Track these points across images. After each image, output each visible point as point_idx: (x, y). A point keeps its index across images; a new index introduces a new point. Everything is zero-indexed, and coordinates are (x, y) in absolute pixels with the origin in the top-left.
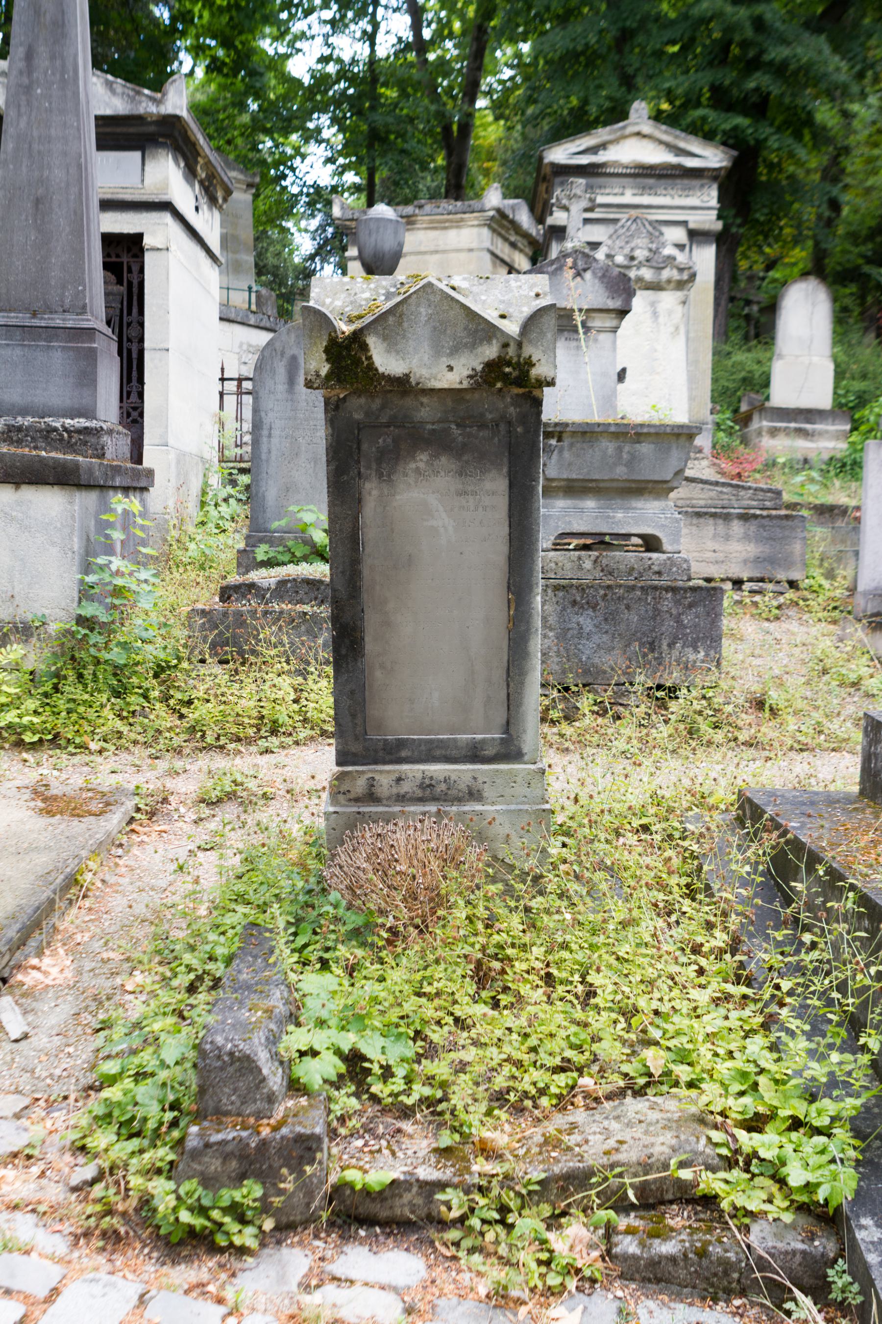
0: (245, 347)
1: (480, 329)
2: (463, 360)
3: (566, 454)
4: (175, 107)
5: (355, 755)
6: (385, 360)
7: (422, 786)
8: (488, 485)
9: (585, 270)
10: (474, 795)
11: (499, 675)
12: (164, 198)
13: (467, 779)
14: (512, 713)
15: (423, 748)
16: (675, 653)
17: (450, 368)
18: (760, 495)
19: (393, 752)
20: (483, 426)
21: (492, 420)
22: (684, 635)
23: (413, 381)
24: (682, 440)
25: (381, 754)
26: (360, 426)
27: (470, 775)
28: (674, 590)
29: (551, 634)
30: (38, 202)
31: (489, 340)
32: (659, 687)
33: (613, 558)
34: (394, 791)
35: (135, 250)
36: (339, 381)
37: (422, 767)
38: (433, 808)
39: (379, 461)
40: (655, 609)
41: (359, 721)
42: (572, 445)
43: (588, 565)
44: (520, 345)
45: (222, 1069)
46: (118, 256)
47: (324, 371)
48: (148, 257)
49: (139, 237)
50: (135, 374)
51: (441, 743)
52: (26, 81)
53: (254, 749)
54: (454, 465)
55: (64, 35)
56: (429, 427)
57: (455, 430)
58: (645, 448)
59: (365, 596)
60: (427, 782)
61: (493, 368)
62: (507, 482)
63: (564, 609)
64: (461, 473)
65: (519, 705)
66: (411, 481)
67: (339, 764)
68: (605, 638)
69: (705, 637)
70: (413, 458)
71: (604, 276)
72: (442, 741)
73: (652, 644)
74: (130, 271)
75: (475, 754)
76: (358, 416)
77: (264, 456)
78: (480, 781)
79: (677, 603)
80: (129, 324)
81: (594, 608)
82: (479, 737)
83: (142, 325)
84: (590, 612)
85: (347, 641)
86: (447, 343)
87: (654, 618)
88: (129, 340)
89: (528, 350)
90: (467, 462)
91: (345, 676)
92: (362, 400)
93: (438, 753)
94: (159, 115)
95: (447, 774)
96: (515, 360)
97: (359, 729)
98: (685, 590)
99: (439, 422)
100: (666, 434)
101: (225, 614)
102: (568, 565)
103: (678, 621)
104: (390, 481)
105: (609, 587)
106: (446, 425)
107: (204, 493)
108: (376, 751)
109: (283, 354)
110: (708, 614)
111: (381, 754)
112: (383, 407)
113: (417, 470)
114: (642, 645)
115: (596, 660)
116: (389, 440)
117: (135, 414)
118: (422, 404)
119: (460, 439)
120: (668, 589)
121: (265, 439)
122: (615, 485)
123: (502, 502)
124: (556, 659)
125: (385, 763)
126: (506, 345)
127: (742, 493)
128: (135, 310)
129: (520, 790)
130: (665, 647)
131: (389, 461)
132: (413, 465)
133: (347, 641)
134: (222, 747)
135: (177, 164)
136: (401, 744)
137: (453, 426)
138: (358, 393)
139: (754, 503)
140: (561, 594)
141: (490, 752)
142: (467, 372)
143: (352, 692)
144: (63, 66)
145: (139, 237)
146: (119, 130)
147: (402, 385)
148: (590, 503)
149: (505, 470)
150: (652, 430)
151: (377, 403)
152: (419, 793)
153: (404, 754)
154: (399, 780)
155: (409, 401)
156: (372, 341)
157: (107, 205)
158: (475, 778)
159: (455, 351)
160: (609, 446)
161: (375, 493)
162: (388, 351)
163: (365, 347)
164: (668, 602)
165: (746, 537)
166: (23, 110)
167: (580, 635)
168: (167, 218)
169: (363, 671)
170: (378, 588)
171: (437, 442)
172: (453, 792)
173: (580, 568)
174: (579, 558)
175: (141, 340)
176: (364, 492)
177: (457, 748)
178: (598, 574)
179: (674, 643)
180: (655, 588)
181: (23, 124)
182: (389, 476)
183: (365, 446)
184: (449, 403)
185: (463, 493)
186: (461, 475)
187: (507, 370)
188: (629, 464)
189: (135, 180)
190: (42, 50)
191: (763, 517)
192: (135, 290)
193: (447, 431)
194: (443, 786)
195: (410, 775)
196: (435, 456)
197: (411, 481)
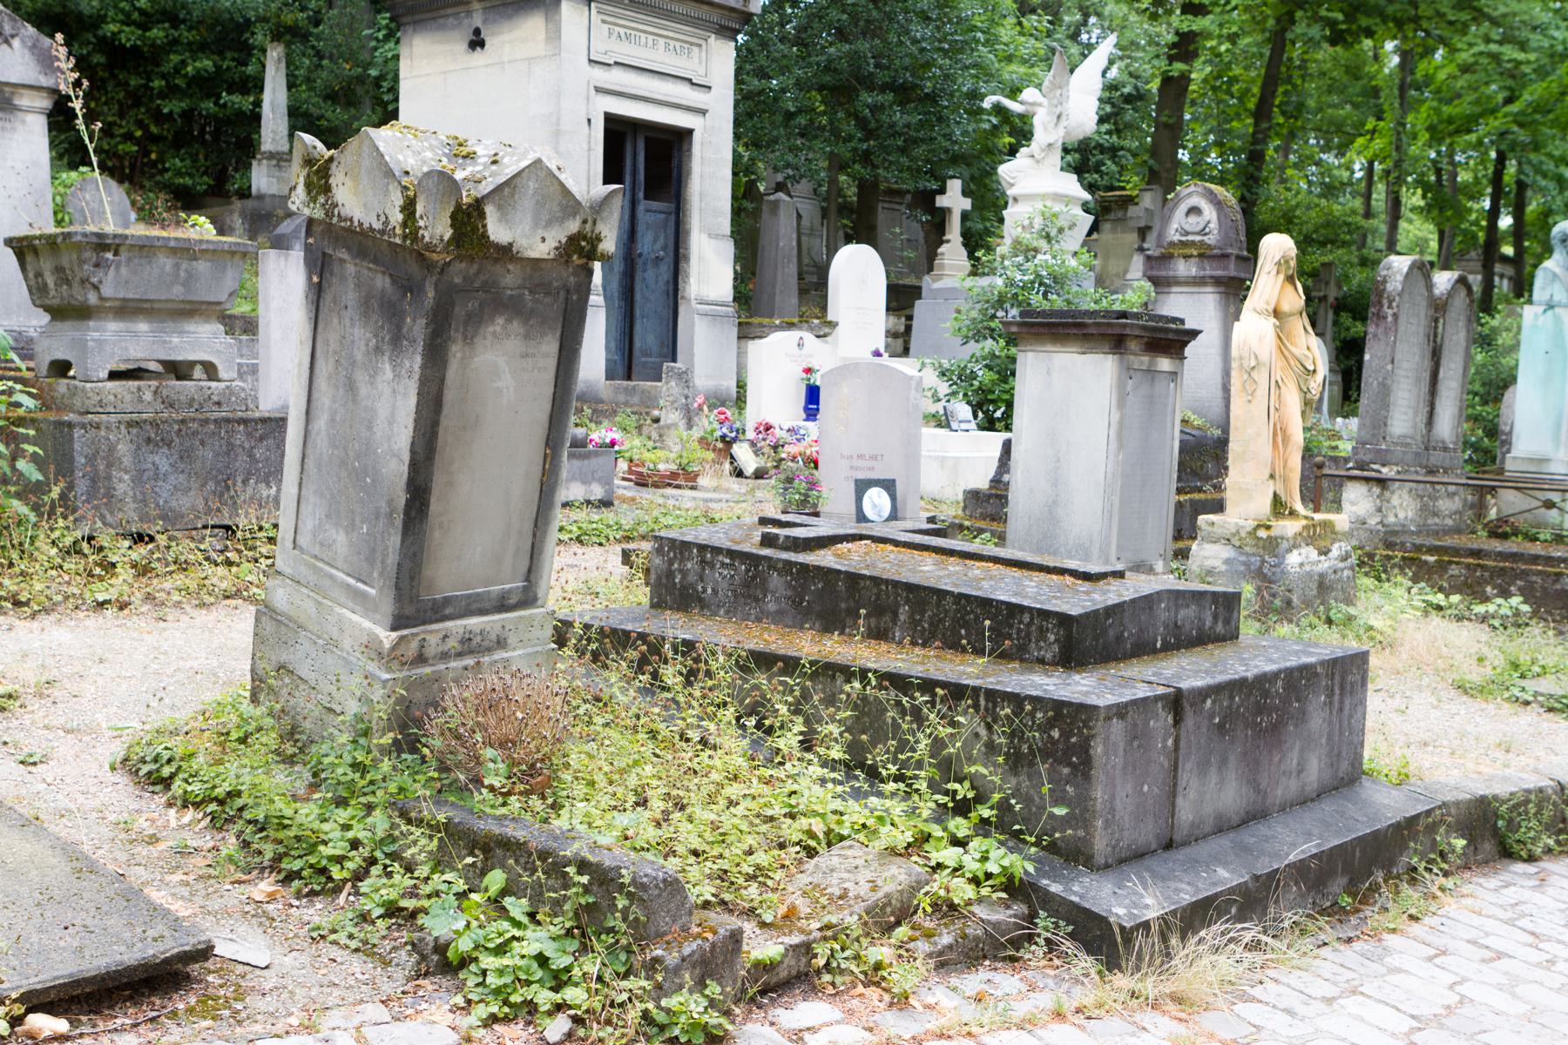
2: (553, 233)
3: (123, 270)
5: (408, 618)
6: (497, 230)
7: (462, 642)
9: (13, 36)
10: (501, 643)
13: (497, 629)
16: (249, 491)
17: (543, 239)
19: (438, 611)
20: (548, 294)
22: (258, 470)
29: (126, 477)
31: (574, 215)
33: (173, 388)
34: (440, 649)
39: (466, 324)
40: (229, 444)
42: (129, 260)
43: (148, 396)
45: (659, 896)
57: (528, 296)
58: (202, 266)
63: (138, 448)
64: (527, 337)
65: (541, 553)
68: (182, 478)
70: (493, 321)
71: (34, 46)
72: (478, 594)
75: (502, 605)
76: (457, 280)
79: (249, 435)
81: (169, 446)
82: (507, 586)
84: (165, 450)
86: (545, 216)
87: (228, 453)
92: (463, 265)
93: (474, 606)
94: (1272, 105)
102: (128, 398)
104: (472, 343)
105: (183, 421)
111: (429, 613)
112: (479, 272)
114: (218, 483)
115: (174, 504)
122: (169, 306)
123: (551, 364)
124: (133, 506)
130: (239, 484)
131: (475, 321)
132: (491, 329)
136: (447, 601)
140: (134, 431)
147: (506, 252)
148: (143, 326)
149: (558, 334)
150: (211, 247)
151: (475, 266)
152: (459, 647)
153: (447, 611)
154: (446, 637)
159: (549, 224)
160: (165, 262)
161: (459, 355)
163: (482, 215)
167: (156, 477)
171: (511, 307)
172: (486, 643)
173: (140, 400)
174: (139, 389)
178: (159, 407)
184: (528, 270)
185: (525, 356)
188: (186, 283)
193: (521, 296)
196: (509, 321)
197: (488, 343)
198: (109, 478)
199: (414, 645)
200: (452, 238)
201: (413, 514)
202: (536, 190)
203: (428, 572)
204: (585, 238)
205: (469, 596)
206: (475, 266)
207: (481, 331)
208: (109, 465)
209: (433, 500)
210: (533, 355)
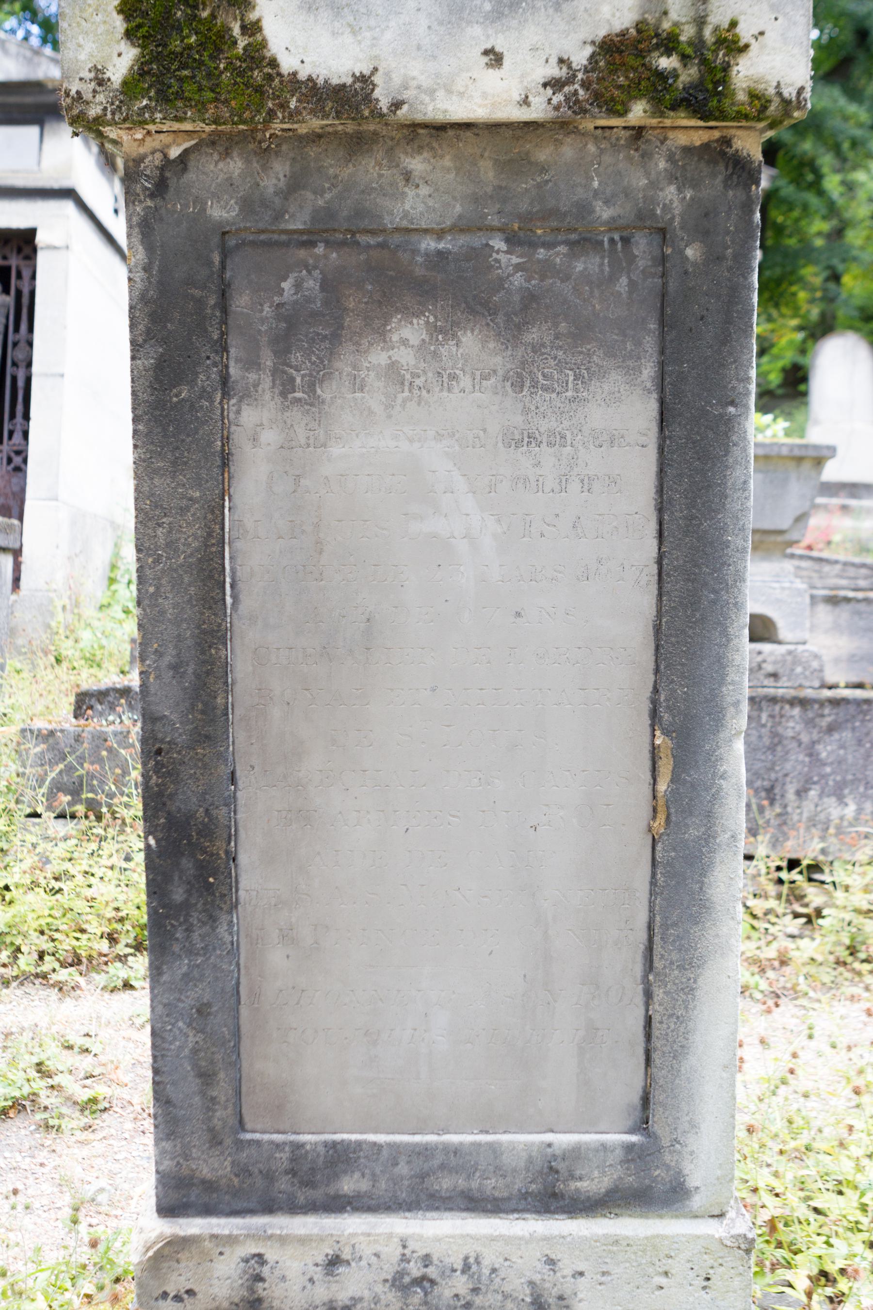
2: (532, 34)
5: (209, 1186)
12: (65, 184)
14: (660, 1073)
15: (403, 1169)
16: (808, 807)
18: (852, 572)
19: (316, 1181)
20: (584, 243)
21: (613, 225)
22: (823, 776)
23: (382, 97)
24: (807, 465)
25: (283, 1184)
28: (803, 703)
32: (793, 864)
35: (27, 250)
36: (164, 97)
39: (283, 344)
40: (774, 734)
41: (222, 1090)
48: (42, 258)
49: (30, 234)
50: (20, 408)
51: (455, 1159)
53: (100, 979)
54: (499, 361)
56: (429, 244)
59: (239, 736)
60: (415, 1270)
62: (652, 406)
64: (519, 380)
65: (679, 1052)
67: (168, 1209)
69: (856, 781)
70: (382, 334)
72: (456, 1150)
73: (770, 790)
74: (19, 276)
75: (551, 1192)
76: (221, 212)
78: (567, 1267)
79: (810, 723)
80: (15, 344)
82: (563, 1140)
83: (30, 344)
85: (186, 863)
87: (772, 748)
88: (15, 364)
90: (537, 348)
91: (183, 966)
92: (235, 166)
93: (445, 1183)
95: (470, 1249)
96: (687, 34)
97: (223, 1115)
98: (822, 703)
99: (459, 228)
100: (780, 457)
101: (78, 738)
103: (812, 753)
104: (313, 401)
106: (477, 240)
107: (113, 567)
108: (269, 1177)
110: (860, 742)
111: (283, 1184)
112: (295, 185)
116: (312, 285)
117: (17, 460)
118: (407, 176)
119: (518, 280)
120: (794, 702)
123: (636, 467)
125: (294, 1208)
127: (827, 568)
128: (24, 327)
130: (791, 796)
131: (310, 343)
132: (379, 357)
133: (186, 863)
134: (44, 976)
136: (341, 1157)
137: (498, 244)
138: (220, 144)
139: (844, 582)
141: (593, 1183)
143: (203, 1010)
145: (30, 234)
149: (648, 371)
151: (279, 171)
153: (348, 1185)
154: (334, 1262)
155: (370, 169)
158: (551, 1262)
161: (270, 437)
164: (793, 723)
165: (836, 628)
168: (68, 207)
169: (234, 951)
170: (276, 712)
171: (446, 287)
175: (29, 364)
176: (239, 436)
177: (499, 1171)
179: (806, 790)
180: (773, 700)
182: (311, 388)
183: (241, 302)
184: (488, 172)
186: (518, 385)
187: (665, 63)
191: (858, 601)
192: (25, 301)
194: (460, 1284)
195: (367, 1251)
196: (445, 331)
200: (140, 74)
201: (178, 894)
203: (263, 1064)
205: (424, 1152)
207: (343, 365)
210: (557, 439)
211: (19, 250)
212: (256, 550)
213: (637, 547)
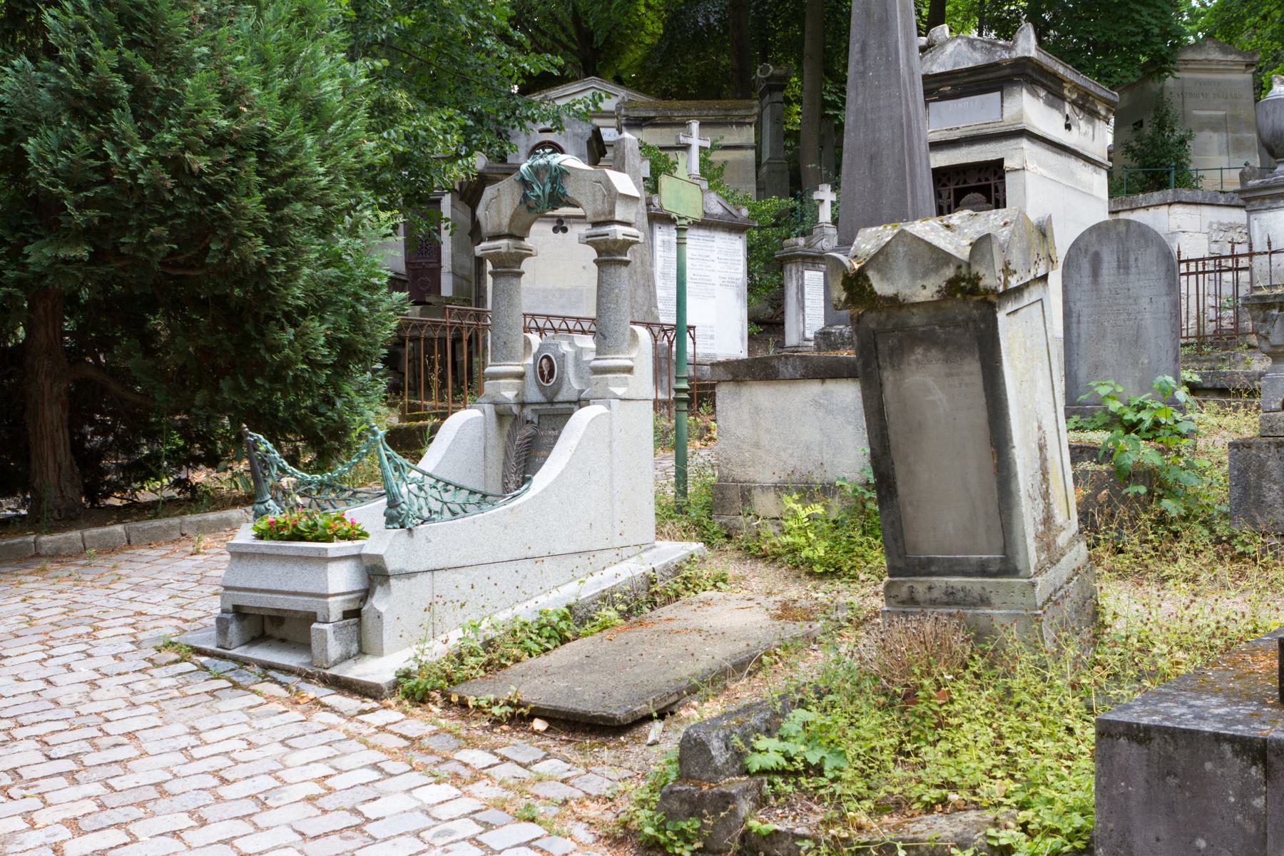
0: (1215, 226)
1: (940, 257)
2: (932, 281)
4: (1024, 50)
5: (900, 569)
6: (882, 287)
8: (967, 368)
10: (984, 601)
11: (993, 509)
12: (1019, 127)
13: (977, 589)
19: (925, 568)
20: (957, 325)
23: (901, 299)
26: (874, 332)
27: (980, 585)
30: (872, 157)
34: (928, 596)
37: (945, 579)
38: (954, 611)
39: (891, 356)
41: (900, 544)
44: (969, 265)
45: (690, 749)
46: (987, 180)
47: (843, 298)
48: (1008, 177)
49: (1000, 162)
52: (861, 68)
55: (888, 28)
59: (893, 452)
61: (953, 284)
64: (947, 361)
66: (914, 368)
74: (997, 191)
75: (983, 570)
76: (873, 326)
77: (1074, 340)
78: (988, 590)
82: (985, 556)
89: (976, 269)
92: (874, 314)
93: (957, 568)
94: (1011, 59)
104: (900, 370)
109: (1086, 251)
112: (888, 317)
113: (917, 361)
121: (1075, 326)
123: (978, 380)
126: (959, 267)
129: (1018, 598)
131: (898, 354)
132: (913, 357)
135: (1035, 94)
136: (931, 561)
141: (994, 568)
142: (935, 289)
143: (893, 522)
144: (888, 51)
145: (1000, 162)
146: (981, 77)
147: (894, 302)
151: (884, 314)
152: (945, 599)
153: (933, 569)
154: (930, 588)
155: (904, 312)
156: (870, 273)
157: (936, 146)
159: (925, 275)
161: (891, 378)
162: (882, 280)
163: (866, 279)
166: (860, 90)
168: (1025, 143)
171: (927, 339)
172: (969, 599)
176: (884, 379)
181: (859, 102)
183: (880, 346)
185: (949, 375)
189: (996, 117)
190: (872, 42)
194: (962, 594)
196: (927, 350)
197: (914, 368)
198: (1259, 487)
199: (905, 589)
202: (906, 253)
204: (963, 280)
206: (884, 314)
208: (1260, 477)
209: (899, 484)
210: (958, 375)
211: (996, 174)
212: (891, 408)
213: (982, 401)
